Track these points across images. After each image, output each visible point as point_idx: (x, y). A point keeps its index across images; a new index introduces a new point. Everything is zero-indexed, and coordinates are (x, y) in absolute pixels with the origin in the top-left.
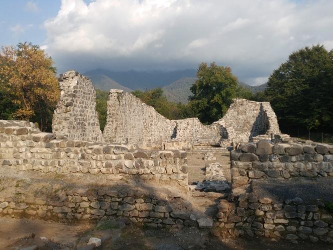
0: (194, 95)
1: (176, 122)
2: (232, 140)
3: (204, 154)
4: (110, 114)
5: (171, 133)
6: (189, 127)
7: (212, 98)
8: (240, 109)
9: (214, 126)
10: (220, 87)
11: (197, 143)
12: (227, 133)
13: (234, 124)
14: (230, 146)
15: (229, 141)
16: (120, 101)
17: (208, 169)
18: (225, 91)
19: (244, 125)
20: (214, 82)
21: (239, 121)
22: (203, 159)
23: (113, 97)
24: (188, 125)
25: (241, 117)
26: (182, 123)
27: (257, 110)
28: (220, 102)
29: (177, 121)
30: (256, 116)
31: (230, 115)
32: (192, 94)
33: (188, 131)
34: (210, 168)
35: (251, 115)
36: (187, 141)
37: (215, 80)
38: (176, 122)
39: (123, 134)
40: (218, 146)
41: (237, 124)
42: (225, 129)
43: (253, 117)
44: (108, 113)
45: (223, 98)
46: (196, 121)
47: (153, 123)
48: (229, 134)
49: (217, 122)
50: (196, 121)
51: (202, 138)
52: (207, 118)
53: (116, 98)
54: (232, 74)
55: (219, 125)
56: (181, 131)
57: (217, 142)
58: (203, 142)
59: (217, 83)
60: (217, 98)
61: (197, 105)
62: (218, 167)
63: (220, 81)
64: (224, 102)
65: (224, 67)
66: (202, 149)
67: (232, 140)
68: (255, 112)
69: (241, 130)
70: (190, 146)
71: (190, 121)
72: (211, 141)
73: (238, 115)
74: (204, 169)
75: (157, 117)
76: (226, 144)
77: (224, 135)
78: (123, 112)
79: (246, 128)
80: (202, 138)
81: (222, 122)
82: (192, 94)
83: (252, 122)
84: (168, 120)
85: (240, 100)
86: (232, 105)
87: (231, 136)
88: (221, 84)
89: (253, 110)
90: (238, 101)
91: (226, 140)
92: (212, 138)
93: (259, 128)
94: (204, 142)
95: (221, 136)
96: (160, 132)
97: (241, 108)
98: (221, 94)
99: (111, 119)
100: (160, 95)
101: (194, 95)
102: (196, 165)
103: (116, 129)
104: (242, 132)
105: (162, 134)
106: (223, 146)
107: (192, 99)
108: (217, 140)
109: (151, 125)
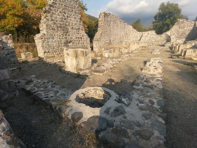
0: (155, 20)
1: (142, 33)
2: (173, 43)
3: (153, 50)
4: (100, 26)
5: (139, 38)
6: (149, 35)
7: (165, 21)
8: (181, 25)
9: (164, 35)
10: (170, 14)
11: (152, 44)
12: (170, 39)
13: (176, 34)
14: (171, 46)
15: (170, 43)
16: (106, 18)
17: (148, 63)
18: (173, 17)
19: (182, 35)
20: (168, 12)
21: (179, 32)
22: (151, 53)
23: (102, 16)
24: (148, 34)
25: (181, 30)
26: (145, 34)
27: (192, 26)
28: (169, 23)
29: (143, 33)
30: (190, 30)
31: (174, 29)
32: (154, 20)
33: (147, 38)
34: (151, 63)
35: (187, 29)
36: (145, 43)
37: (168, 11)
38: (142, 33)
39: (107, 37)
40: (163, 46)
41: (178, 34)
42: (170, 37)
43: (189, 30)
44: (99, 25)
45: (171, 21)
46: (153, 32)
47: (131, 34)
48: (172, 40)
49: (165, 33)
50: (153, 32)
51: (155, 41)
52: (159, 32)
53: (103, 16)
54: (178, 8)
55: (166, 34)
56: (144, 38)
57: (163, 44)
58: (155, 44)
59: (169, 12)
60: (168, 21)
61: (156, 26)
62: (158, 62)
63: (171, 11)
64: (171, 23)
65: (175, 4)
66: (153, 47)
67: (173, 43)
68: (190, 27)
69: (179, 38)
70: (147, 45)
71: (150, 33)
72: (160, 43)
73: (179, 29)
74: (145, 63)
75: (133, 31)
76: (169, 45)
77: (168, 40)
78: (108, 25)
79: (182, 36)
80: (155, 41)
81: (168, 33)
82: (154, 20)
83: (187, 33)
84: (138, 32)
85: (182, 20)
86: (177, 23)
87: (172, 41)
88: (171, 13)
89: (189, 26)
90: (181, 20)
91: (169, 43)
92: (161, 42)
93: (190, 37)
94: (155, 43)
95: (166, 41)
96: (133, 38)
97: (182, 25)
98: (170, 19)
99: (100, 29)
100: (139, 22)
101: (155, 20)
102: (144, 57)
103: (101, 34)
104: (179, 39)
105: (134, 39)
106: (166, 46)
107: (154, 23)
108: (163, 43)
109: (130, 35)
